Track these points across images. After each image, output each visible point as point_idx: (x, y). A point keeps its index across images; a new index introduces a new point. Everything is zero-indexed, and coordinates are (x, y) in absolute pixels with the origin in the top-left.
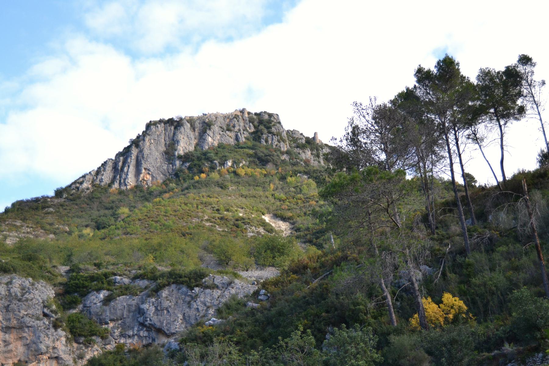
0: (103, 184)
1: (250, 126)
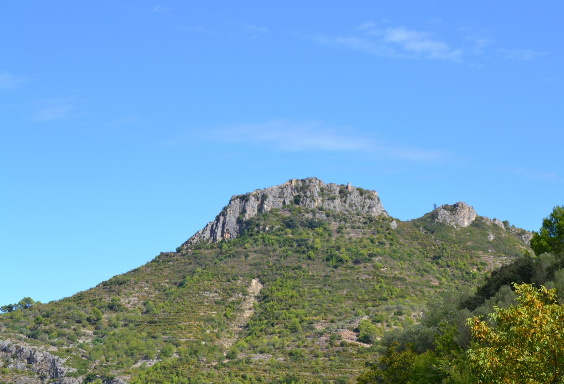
0: (204, 239)
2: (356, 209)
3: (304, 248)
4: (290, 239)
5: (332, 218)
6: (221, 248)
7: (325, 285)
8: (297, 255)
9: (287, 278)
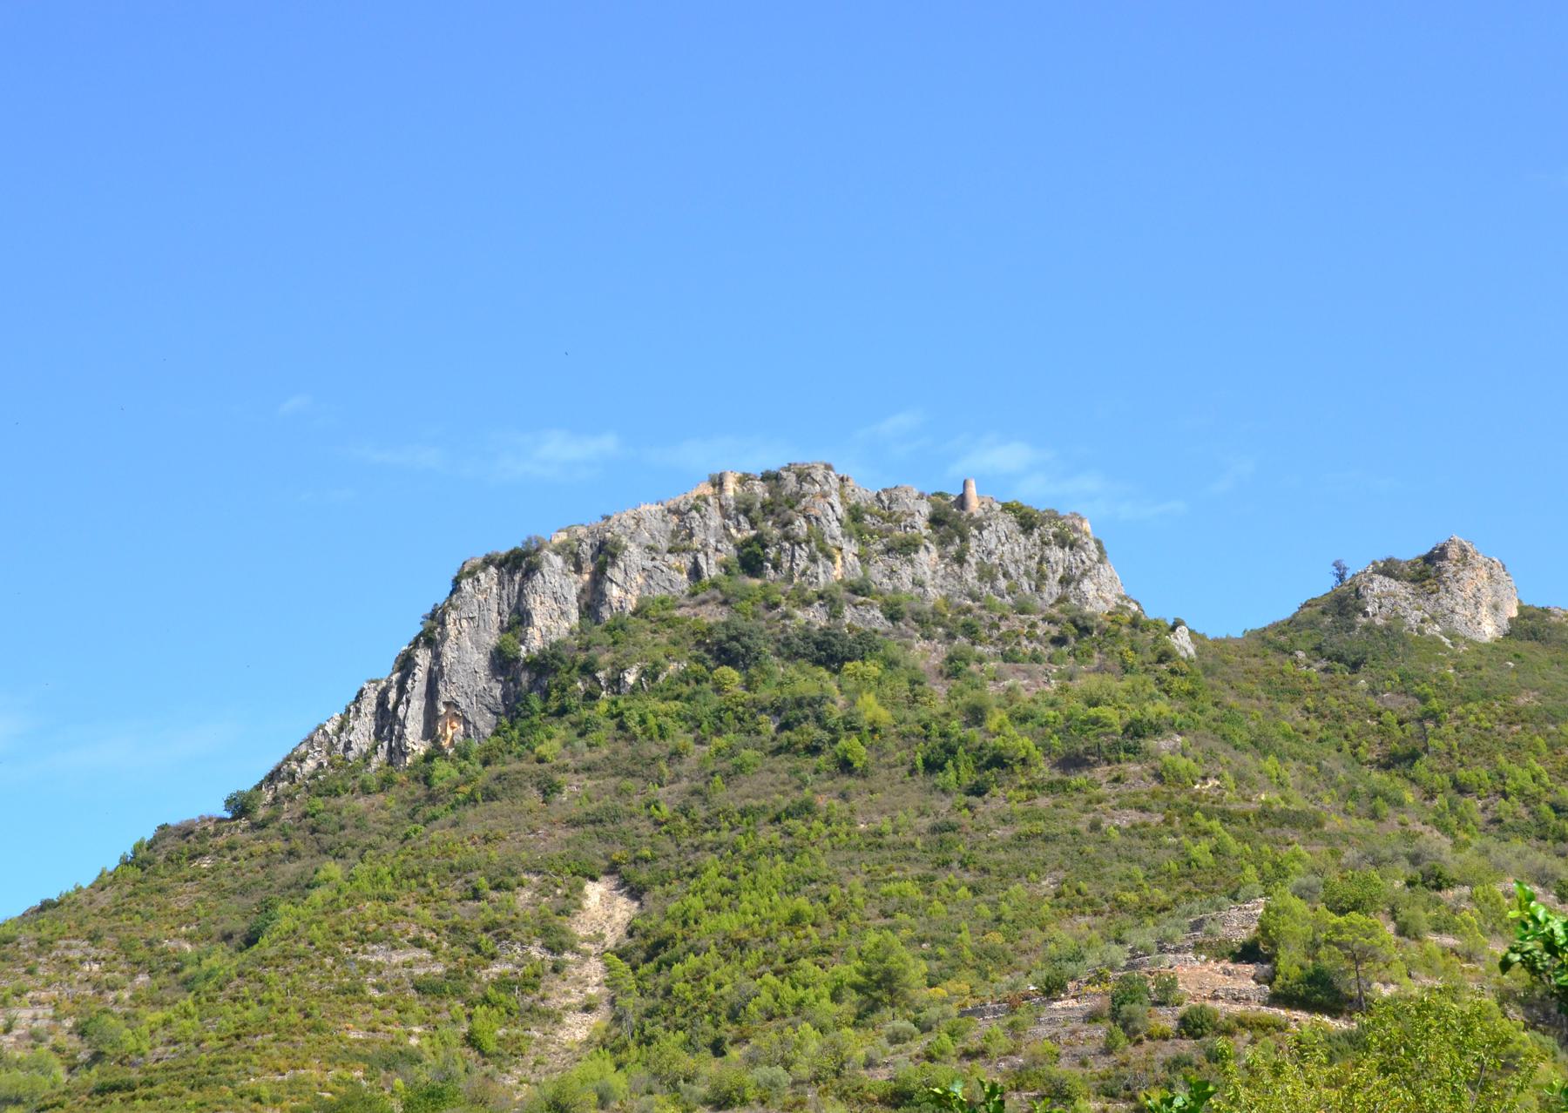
2: (1011, 591)
3: (813, 732)
4: (743, 705)
5: (913, 624)
6: (427, 780)
7: (946, 864)
8: (784, 763)
9: (750, 857)
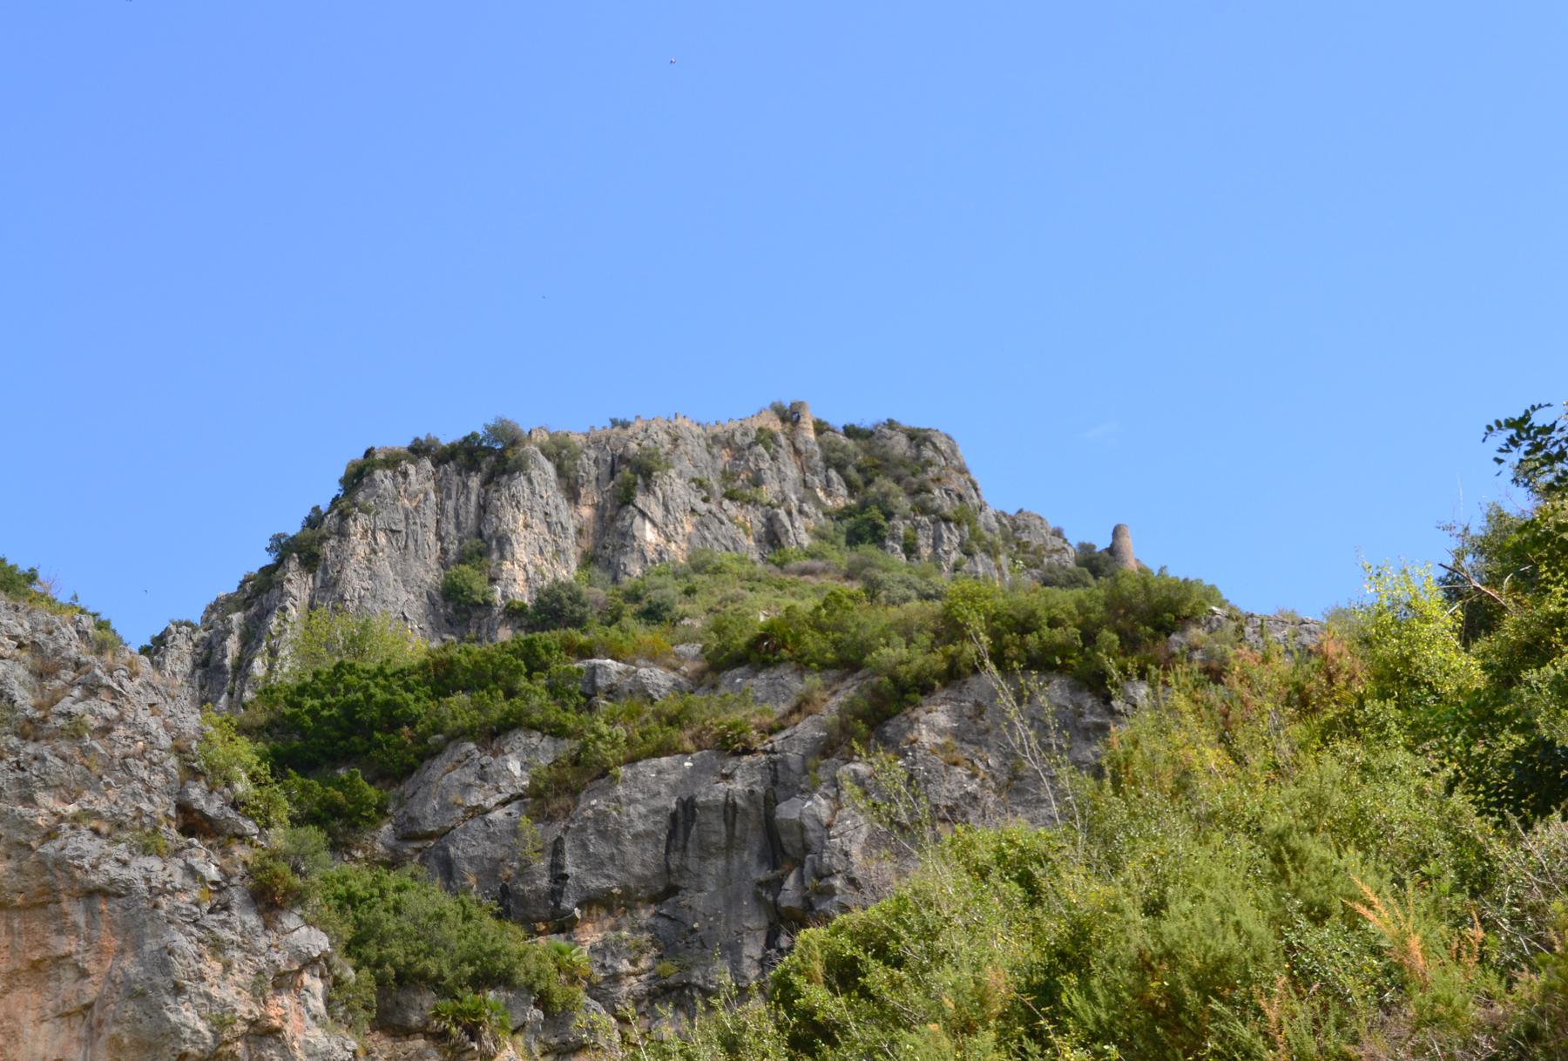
1: (828, 481)
